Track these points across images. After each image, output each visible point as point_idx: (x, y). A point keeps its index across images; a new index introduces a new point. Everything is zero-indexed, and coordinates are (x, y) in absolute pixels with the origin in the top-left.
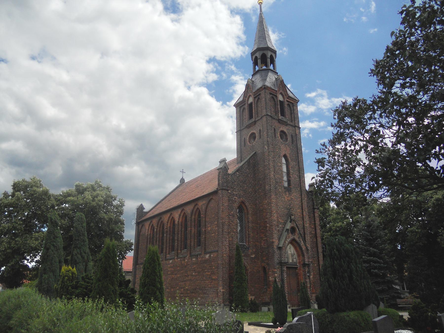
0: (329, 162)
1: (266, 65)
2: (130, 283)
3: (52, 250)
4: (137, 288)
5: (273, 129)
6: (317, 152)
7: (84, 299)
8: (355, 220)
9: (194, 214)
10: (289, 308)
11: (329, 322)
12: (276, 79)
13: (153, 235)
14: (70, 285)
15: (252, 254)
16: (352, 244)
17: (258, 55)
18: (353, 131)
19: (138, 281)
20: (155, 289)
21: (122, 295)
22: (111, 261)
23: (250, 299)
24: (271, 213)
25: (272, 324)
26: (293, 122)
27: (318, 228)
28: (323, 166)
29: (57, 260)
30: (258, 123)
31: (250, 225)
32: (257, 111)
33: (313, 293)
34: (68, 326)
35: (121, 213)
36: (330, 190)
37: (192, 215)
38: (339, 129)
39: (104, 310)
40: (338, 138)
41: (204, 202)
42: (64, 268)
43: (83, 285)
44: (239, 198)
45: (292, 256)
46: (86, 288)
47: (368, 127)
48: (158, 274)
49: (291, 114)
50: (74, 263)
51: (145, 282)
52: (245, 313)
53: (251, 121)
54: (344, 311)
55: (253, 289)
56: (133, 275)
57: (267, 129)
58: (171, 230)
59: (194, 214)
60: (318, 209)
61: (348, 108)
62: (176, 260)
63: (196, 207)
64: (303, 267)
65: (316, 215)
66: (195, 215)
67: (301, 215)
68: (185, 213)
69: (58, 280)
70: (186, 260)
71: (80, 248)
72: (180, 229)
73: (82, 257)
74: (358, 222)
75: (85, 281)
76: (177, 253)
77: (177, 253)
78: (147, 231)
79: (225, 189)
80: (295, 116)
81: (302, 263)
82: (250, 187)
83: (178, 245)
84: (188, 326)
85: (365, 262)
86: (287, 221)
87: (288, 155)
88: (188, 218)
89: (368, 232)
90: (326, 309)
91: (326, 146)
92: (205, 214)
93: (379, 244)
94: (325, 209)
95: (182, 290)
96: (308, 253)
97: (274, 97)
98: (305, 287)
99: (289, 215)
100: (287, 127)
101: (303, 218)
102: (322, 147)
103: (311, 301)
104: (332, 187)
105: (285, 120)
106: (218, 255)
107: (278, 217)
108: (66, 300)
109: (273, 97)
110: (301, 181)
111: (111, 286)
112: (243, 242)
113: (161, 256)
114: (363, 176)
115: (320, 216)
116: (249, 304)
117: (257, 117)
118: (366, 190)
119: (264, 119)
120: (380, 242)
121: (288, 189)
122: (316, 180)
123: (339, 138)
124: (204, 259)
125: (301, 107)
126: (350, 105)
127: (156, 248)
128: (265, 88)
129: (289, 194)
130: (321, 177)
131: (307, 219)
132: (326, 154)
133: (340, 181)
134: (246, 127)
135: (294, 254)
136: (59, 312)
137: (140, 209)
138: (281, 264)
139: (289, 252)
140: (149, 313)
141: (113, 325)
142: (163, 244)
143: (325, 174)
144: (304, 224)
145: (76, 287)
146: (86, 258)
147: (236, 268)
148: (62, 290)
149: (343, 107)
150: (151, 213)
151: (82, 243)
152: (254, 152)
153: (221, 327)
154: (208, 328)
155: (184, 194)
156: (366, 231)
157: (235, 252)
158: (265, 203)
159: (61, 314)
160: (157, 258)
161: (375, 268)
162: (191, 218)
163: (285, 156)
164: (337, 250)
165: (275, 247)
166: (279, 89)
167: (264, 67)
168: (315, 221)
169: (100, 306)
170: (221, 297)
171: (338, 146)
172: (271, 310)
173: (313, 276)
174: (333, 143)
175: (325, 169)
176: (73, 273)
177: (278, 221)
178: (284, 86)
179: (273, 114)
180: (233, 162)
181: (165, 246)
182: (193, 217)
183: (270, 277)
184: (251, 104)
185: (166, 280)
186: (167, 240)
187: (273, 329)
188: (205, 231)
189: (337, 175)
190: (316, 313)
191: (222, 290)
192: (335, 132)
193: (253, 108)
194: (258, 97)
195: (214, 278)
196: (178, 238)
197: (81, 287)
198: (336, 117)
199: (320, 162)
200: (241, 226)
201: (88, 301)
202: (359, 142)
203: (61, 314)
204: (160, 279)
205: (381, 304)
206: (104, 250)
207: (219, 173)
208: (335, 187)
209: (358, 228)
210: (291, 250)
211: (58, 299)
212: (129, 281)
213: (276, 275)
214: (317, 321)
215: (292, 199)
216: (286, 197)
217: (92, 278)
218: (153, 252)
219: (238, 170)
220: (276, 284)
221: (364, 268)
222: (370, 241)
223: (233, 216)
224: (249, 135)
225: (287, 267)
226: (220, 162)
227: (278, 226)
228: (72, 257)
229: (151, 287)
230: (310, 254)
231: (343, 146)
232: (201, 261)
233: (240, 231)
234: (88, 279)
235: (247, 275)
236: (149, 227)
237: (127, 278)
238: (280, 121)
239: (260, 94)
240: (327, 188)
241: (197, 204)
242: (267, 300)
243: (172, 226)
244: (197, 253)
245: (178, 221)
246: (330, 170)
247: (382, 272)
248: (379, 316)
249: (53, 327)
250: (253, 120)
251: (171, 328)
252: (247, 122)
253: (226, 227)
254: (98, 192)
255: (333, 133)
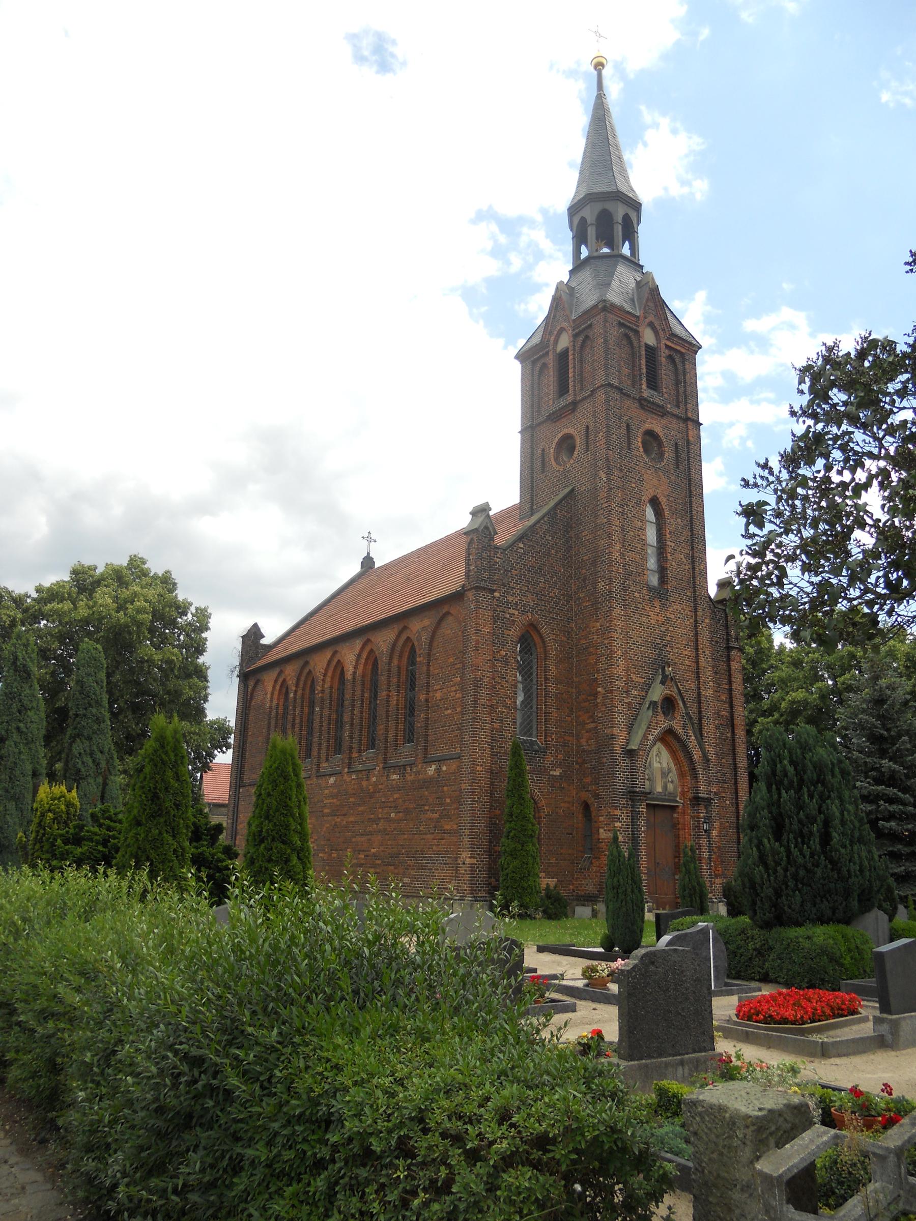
0: (778, 514)
1: (610, 244)
2: (221, 832)
3: (15, 743)
4: (241, 846)
5: (625, 425)
6: (746, 484)
7: (95, 871)
8: (843, 683)
9: (397, 654)
10: (649, 911)
11: (754, 950)
12: (638, 283)
13: (286, 708)
14: (61, 835)
15: (554, 766)
16: (833, 745)
17: (590, 214)
18: (850, 429)
19: (243, 828)
20: (289, 851)
21: (199, 861)
22: (170, 773)
23: (544, 886)
24: (610, 657)
25: (601, 950)
26: (682, 405)
27: (739, 700)
28: (761, 526)
29: (29, 768)
30: (582, 408)
31: (552, 689)
32: (581, 374)
33: (716, 876)
34: (52, 936)
35: (200, 649)
36: (775, 592)
37: (391, 658)
38: (810, 422)
39: (149, 897)
40: (808, 448)
41: (426, 622)
42: (44, 790)
43: (96, 834)
44: (524, 612)
45: (664, 774)
46: (105, 843)
47: (896, 419)
48: (296, 810)
49: (677, 383)
50: (74, 778)
51: (261, 831)
52: (528, 921)
53: (562, 402)
54: (799, 924)
55: (553, 860)
56: (231, 814)
57: (608, 426)
58: (335, 696)
59: (397, 654)
60: (741, 650)
61: (839, 364)
62: (346, 777)
63: (403, 637)
64: (693, 806)
65: (735, 665)
66: (401, 657)
67: (693, 664)
68: (372, 650)
69: (30, 822)
70: (374, 779)
71: (89, 738)
72: (358, 693)
73: (94, 761)
74: (849, 688)
75: (100, 826)
76: (350, 758)
77: (350, 758)
78: (269, 696)
79: (484, 589)
80: (689, 389)
81: (690, 795)
82: (555, 583)
83: (351, 738)
84: (371, 944)
85: (866, 798)
86: (653, 680)
87: (663, 500)
88: (382, 665)
89: (879, 717)
90: (750, 918)
91: (771, 469)
92: (429, 655)
93: (907, 750)
94: (760, 651)
95: (362, 856)
96: (707, 769)
97: (631, 334)
98: (695, 858)
99: (660, 666)
100: (664, 421)
101: (698, 673)
102: (759, 471)
103: (710, 895)
104: (780, 584)
105: (658, 400)
106: (460, 767)
107: (627, 670)
108: (46, 874)
109: (626, 335)
110: (697, 572)
111: (170, 838)
112: (530, 735)
113: (305, 768)
114: (873, 554)
115: (744, 669)
116: (542, 899)
117: (582, 389)
118: (879, 596)
119: (601, 396)
120: (909, 746)
121: (660, 593)
122: (739, 565)
123: (808, 448)
124: (421, 776)
125: (709, 371)
126: (849, 354)
127: (290, 742)
128: (605, 308)
129: (663, 606)
130: (754, 554)
131: (707, 674)
132: (770, 490)
133: (805, 568)
134: (549, 417)
135: (670, 771)
136: (28, 900)
137: (253, 636)
138: (633, 796)
139: (656, 765)
140: (266, 908)
141: (172, 936)
142: (310, 733)
143: (766, 545)
144: (699, 689)
145: (77, 841)
146: (103, 765)
147: (508, 802)
148: (37, 847)
149: (827, 360)
150: (280, 647)
151: (95, 727)
152: (571, 488)
153: (462, 952)
154: (424, 953)
155: (371, 599)
156: (871, 714)
157: (508, 763)
158: (594, 630)
159: (35, 906)
160: (294, 770)
161: (891, 817)
162: (390, 664)
163: (655, 502)
164: (792, 762)
165: (618, 749)
166: (646, 312)
167: (606, 250)
168: (730, 683)
169: (138, 889)
170: (467, 877)
171: (803, 471)
172: (599, 915)
173: (720, 832)
174: (791, 460)
175: (765, 531)
176: (69, 804)
177: (629, 681)
178: (661, 306)
179: (626, 385)
180: (507, 514)
181: (316, 739)
182: (395, 662)
183: (601, 830)
184: (565, 353)
185: (316, 828)
186: (321, 722)
187: (603, 963)
188: (427, 700)
189: (798, 552)
190: (721, 925)
191: (468, 861)
192: (800, 429)
193: (571, 366)
194: (585, 333)
195: (448, 827)
196: (352, 719)
197: (91, 840)
198: (805, 387)
199: (753, 514)
200: (527, 690)
201: (106, 876)
202: (868, 462)
203: (35, 906)
204: (300, 824)
205: (901, 908)
206: (149, 745)
207: (470, 543)
208: (791, 583)
209: (849, 706)
210: (660, 760)
211: (25, 867)
212: (219, 828)
213: (618, 824)
214: (724, 948)
215: (669, 619)
216: (654, 615)
217: (120, 816)
218: (283, 752)
219: (521, 538)
220: (618, 847)
221: (864, 815)
222: (881, 743)
223: (506, 662)
224: (556, 440)
225: (648, 805)
226: (475, 513)
227: (627, 692)
228: (66, 763)
229: (278, 845)
230: (714, 769)
231: (818, 472)
232: (413, 782)
233: (523, 702)
234: (110, 818)
235: (539, 824)
236: (274, 687)
237: (215, 820)
238: (644, 404)
239: (590, 326)
240: (769, 585)
241: (405, 628)
242: (591, 889)
243: (336, 686)
244: (403, 761)
245: (355, 673)
246: (780, 535)
247: (910, 826)
248: (892, 940)
249: (12, 939)
250: (569, 398)
251: (328, 947)
252: (551, 404)
253: (484, 693)
254: (137, 589)
255: (794, 435)
